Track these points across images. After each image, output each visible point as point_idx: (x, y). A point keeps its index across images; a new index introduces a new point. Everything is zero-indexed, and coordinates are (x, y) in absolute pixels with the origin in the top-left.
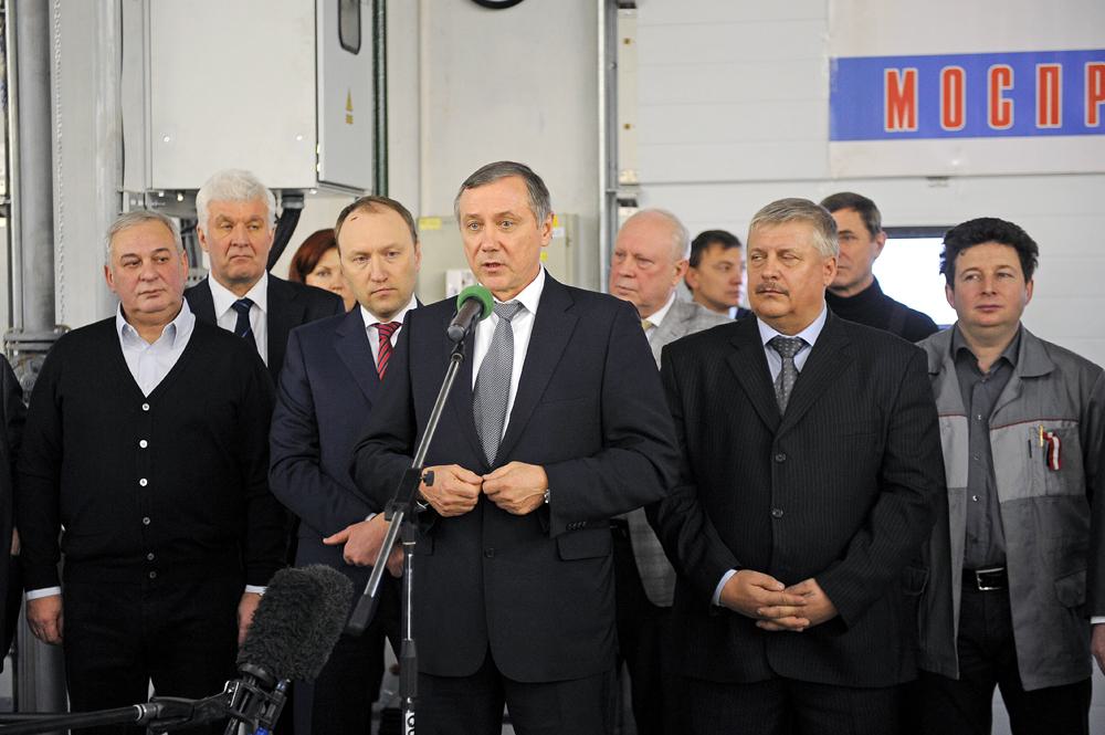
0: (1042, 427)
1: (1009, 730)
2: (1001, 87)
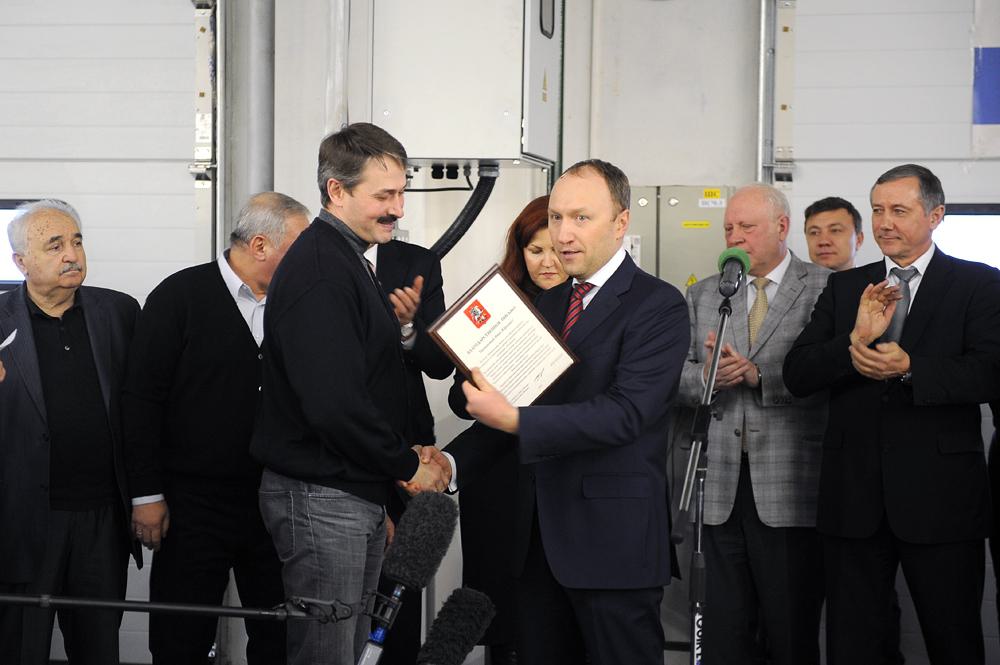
1: (483, 661)
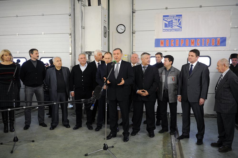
0: (172, 76)
2: (198, 41)
